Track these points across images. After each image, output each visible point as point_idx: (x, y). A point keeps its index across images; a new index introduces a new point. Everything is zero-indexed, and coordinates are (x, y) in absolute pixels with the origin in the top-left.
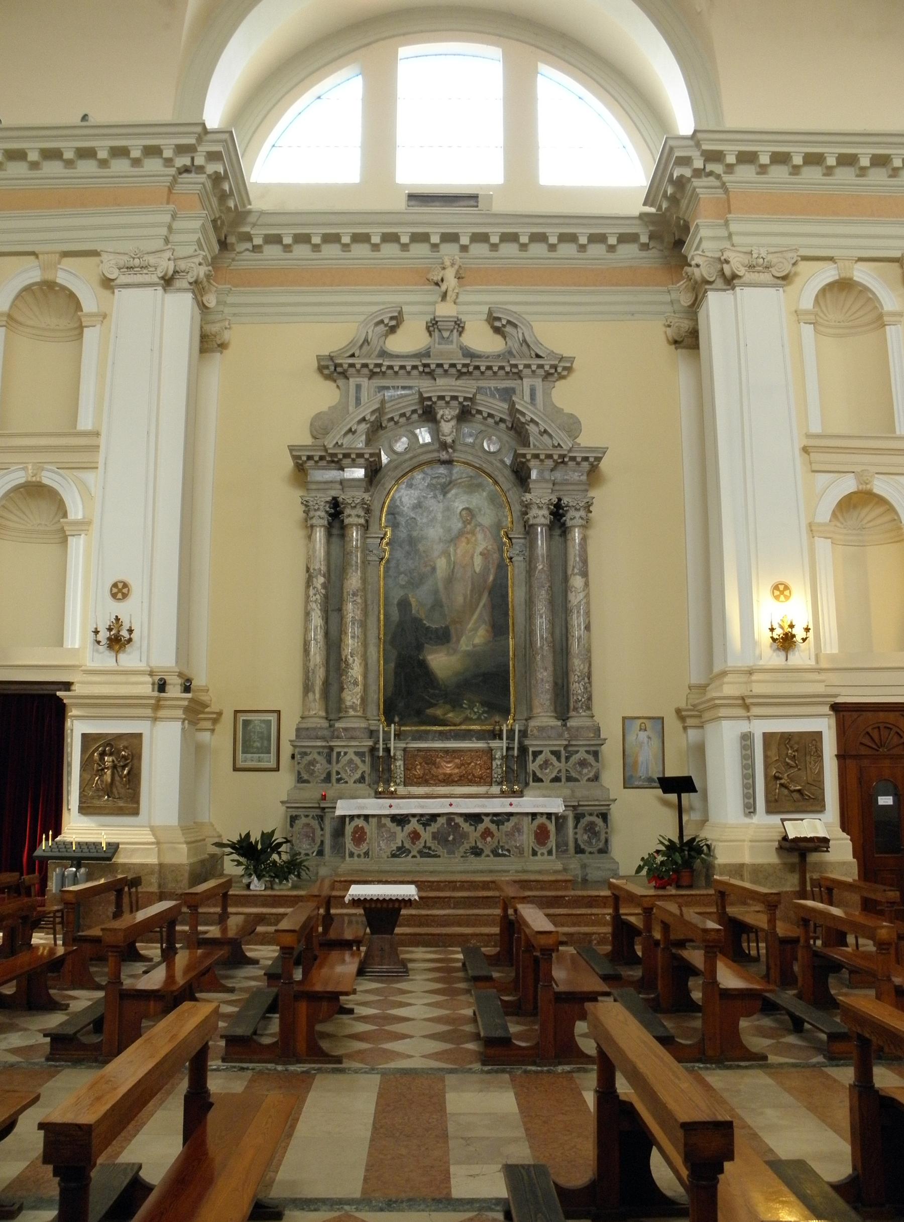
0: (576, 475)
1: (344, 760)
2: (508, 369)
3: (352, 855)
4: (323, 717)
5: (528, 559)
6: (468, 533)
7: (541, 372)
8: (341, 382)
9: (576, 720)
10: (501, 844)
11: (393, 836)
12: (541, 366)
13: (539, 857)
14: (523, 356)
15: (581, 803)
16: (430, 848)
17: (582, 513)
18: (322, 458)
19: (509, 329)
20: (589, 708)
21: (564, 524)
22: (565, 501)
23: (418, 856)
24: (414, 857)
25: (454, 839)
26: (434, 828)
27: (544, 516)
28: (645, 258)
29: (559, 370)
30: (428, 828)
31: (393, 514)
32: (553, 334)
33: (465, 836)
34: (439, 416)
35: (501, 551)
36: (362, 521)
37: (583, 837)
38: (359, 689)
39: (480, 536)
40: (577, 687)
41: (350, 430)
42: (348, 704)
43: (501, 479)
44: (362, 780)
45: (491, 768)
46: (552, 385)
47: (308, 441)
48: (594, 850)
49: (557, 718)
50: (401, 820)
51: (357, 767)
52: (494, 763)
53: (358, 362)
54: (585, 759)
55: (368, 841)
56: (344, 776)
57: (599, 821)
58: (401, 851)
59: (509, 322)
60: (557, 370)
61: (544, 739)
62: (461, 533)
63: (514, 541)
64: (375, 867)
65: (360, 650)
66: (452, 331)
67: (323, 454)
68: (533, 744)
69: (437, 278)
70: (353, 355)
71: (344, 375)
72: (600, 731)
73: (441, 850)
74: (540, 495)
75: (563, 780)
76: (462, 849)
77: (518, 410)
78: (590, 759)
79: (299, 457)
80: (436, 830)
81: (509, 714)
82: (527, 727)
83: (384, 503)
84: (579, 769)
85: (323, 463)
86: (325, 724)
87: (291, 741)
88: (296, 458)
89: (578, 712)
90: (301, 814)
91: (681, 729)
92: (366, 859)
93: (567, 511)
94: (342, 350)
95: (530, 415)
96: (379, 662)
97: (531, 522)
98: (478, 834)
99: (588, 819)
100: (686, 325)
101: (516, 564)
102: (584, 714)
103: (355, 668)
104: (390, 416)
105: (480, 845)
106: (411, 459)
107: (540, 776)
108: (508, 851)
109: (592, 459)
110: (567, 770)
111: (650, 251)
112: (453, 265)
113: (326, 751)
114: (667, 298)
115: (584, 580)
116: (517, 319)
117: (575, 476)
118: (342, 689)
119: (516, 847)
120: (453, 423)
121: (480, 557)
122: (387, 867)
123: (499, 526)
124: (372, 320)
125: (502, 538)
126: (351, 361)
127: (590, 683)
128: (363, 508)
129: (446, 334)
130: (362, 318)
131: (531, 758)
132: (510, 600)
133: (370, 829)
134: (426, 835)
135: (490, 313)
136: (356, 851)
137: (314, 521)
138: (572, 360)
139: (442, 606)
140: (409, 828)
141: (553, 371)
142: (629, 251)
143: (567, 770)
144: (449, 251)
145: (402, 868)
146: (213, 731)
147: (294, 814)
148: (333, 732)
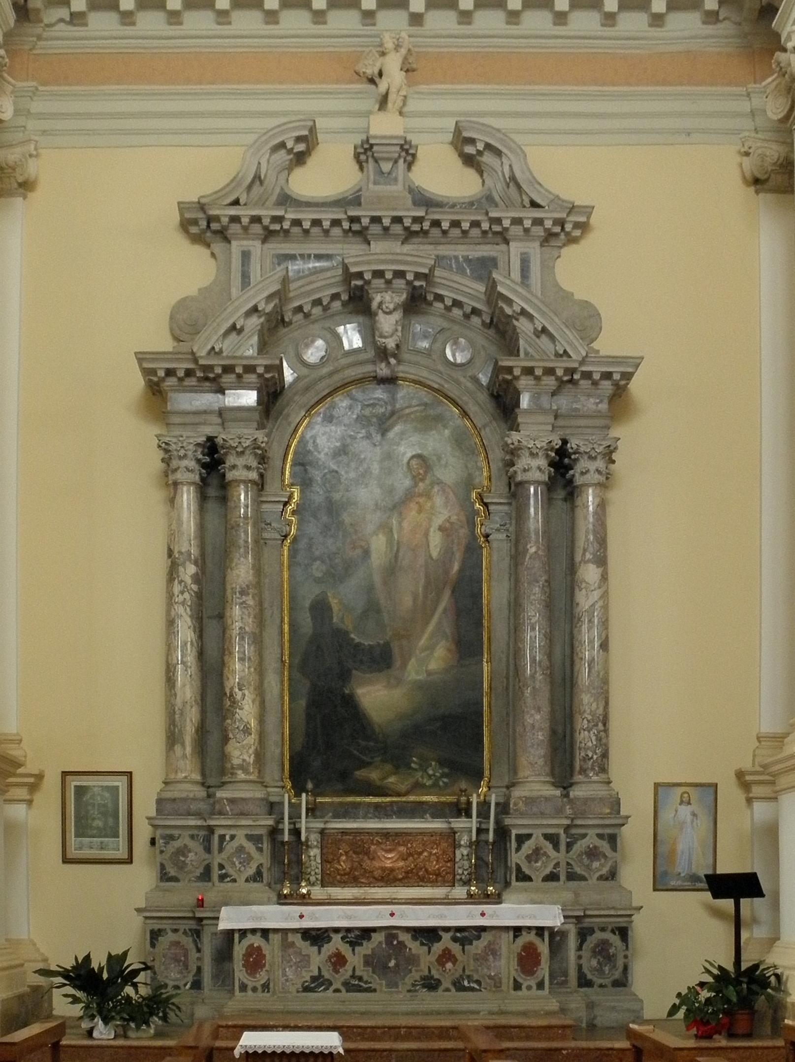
0: (591, 402)
1: (231, 847)
2: (485, 226)
3: (243, 988)
4: (197, 783)
5: (513, 537)
6: (420, 495)
7: (538, 231)
8: (218, 247)
9: (584, 787)
10: (467, 972)
11: (305, 960)
12: (538, 222)
13: (524, 992)
15: (588, 913)
16: (360, 979)
17: (600, 464)
18: (189, 373)
20: (603, 770)
21: (570, 482)
24: (337, 991)
25: (397, 965)
26: (366, 948)
28: (712, 37)
29: (568, 227)
30: (357, 949)
31: (302, 465)
32: (559, 169)
33: (413, 960)
35: (472, 524)
36: (254, 475)
37: (590, 963)
39: (439, 500)
40: (585, 739)
41: (233, 327)
42: (236, 762)
43: (472, 409)
44: (257, 877)
45: (453, 860)
46: (555, 253)
47: (167, 345)
49: (555, 785)
51: (250, 858)
52: (458, 852)
53: (245, 213)
54: (595, 847)
55: (267, 967)
56: (231, 871)
57: (615, 940)
58: (318, 983)
60: (565, 228)
61: (534, 816)
62: (410, 495)
63: (491, 508)
64: (279, 1006)
65: (254, 678)
66: (396, 162)
67: (191, 366)
68: (516, 824)
69: (372, 71)
70: (236, 202)
71: (223, 235)
73: (377, 982)
74: (535, 434)
75: (563, 877)
76: (409, 980)
77: (501, 295)
78: (604, 846)
79: (153, 372)
80: (369, 952)
83: (288, 446)
84: (586, 861)
86: (201, 793)
87: (149, 818)
88: (148, 373)
91: (744, 801)
92: (265, 994)
93: (576, 460)
95: (520, 303)
97: (519, 478)
98: (433, 958)
99: (599, 935)
101: (495, 545)
102: (595, 778)
103: (246, 707)
104: (296, 304)
105: (435, 974)
106: (331, 374)
108: (478, 982)
109: (616, 377)
110: (568, 864)
111: (720, 26)
112: (397, 47)
113: (202, 833)
115: (600, 570)
118: (226, 740)
119: (490, 977)
120: (397, 315)
123: (468, 484)
124: (266, 142)
125: (473, 504)
126: (233, 211)
127: (606, 731)
128: (256, 454)
129: (386, 167)
130: (250, 138)
131: (514, 845)
132: (485, 601)
133: (271, 950)
134: (355, 959)
135: (458, 131)
136: (250, 982)
137: (179, 476)
138: (588, 210)
139: (379, 611)
140: (329, 949)
141: (557, 229)
143: (568, 864)
145: (320, 1007)
146: (30, 802)
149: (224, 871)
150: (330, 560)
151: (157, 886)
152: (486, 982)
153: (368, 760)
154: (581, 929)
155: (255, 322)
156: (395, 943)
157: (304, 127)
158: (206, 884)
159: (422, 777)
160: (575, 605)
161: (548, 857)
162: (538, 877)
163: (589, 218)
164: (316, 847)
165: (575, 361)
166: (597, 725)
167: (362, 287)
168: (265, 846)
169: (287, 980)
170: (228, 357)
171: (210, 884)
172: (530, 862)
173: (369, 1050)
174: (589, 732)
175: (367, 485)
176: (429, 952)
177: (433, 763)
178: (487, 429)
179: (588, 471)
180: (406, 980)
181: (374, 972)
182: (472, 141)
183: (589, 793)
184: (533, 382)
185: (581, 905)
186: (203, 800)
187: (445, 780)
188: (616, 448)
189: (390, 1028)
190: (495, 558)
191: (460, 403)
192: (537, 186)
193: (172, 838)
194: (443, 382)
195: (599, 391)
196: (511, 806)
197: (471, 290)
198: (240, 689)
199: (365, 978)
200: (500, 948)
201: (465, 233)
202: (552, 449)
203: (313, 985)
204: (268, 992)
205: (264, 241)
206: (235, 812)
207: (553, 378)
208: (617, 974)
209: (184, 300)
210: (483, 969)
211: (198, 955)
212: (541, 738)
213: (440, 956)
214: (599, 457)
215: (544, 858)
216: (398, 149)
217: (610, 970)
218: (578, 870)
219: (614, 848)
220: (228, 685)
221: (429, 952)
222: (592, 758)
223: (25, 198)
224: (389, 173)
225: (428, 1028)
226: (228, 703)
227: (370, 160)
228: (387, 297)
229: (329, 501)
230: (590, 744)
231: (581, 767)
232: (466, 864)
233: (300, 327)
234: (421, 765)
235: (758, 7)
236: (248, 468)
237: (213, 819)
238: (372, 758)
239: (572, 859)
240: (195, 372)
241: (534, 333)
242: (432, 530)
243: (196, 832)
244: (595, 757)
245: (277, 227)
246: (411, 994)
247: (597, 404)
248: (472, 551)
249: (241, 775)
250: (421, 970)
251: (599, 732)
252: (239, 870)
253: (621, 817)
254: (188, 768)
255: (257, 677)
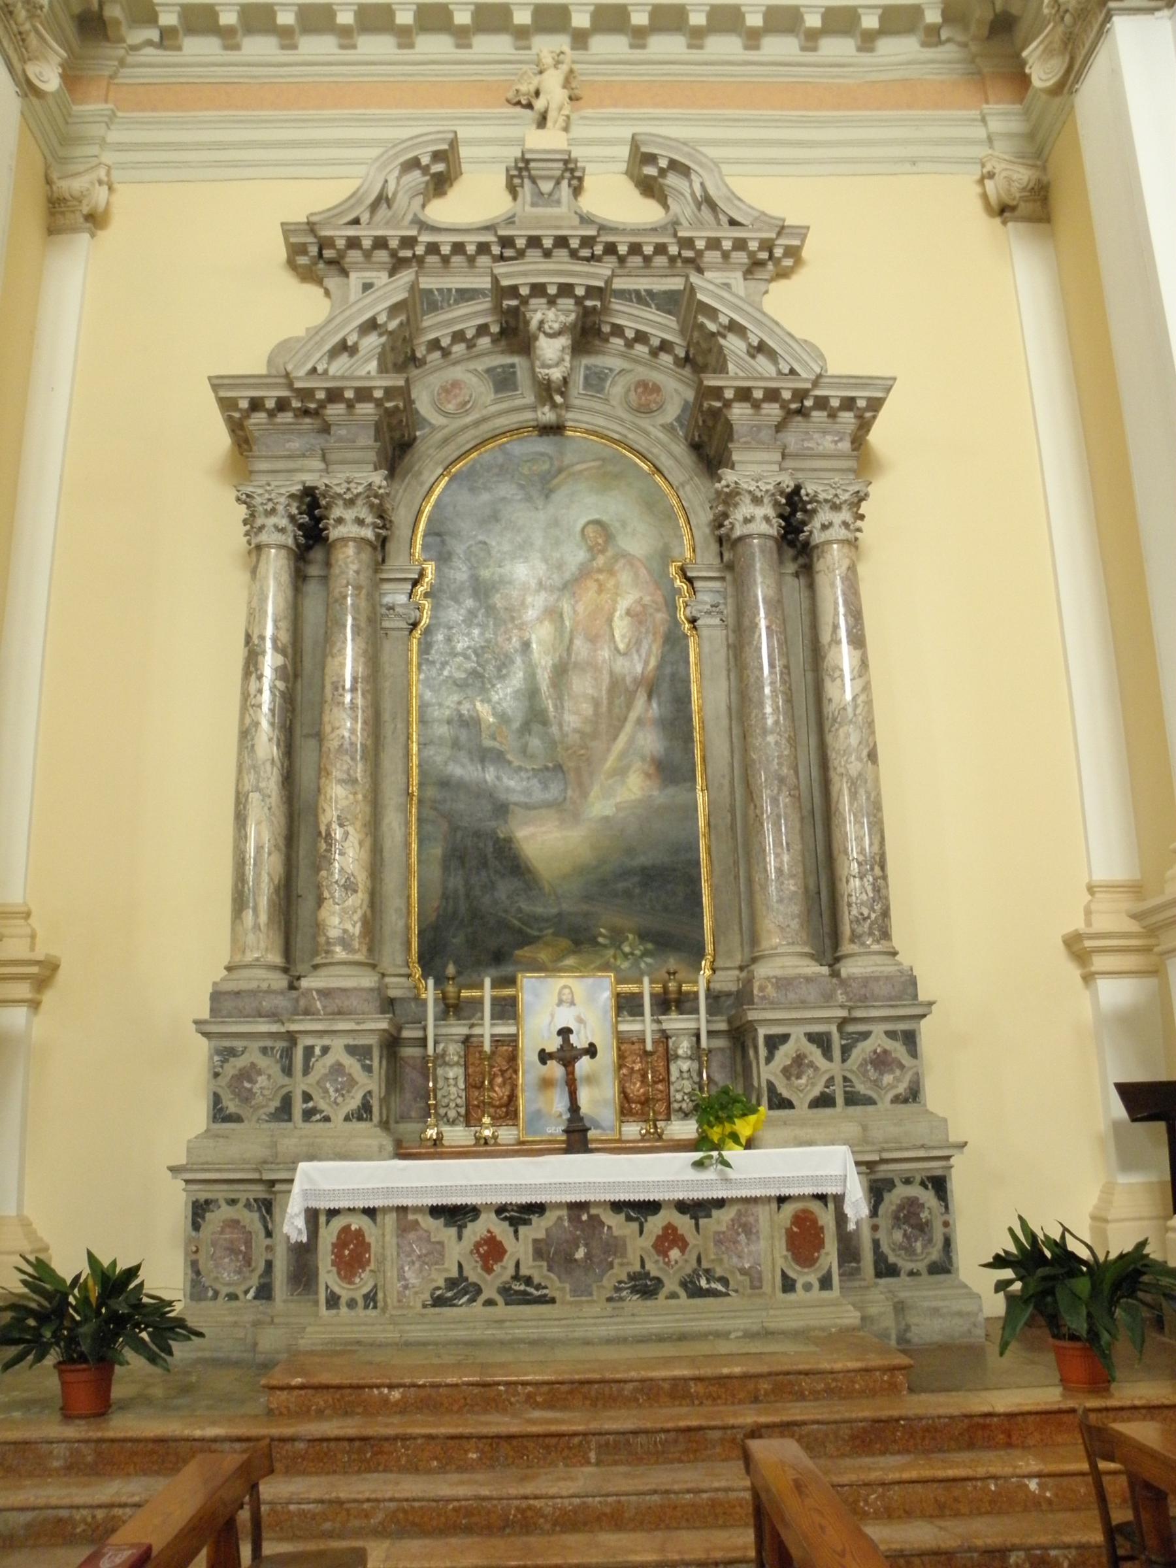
0: (825, 438)
1: (321, 1066)
2: (673, 250)
3: (333, 1301)
4: (273, 968)
5: (731, 621)
6: (600, 571)
7: (741, 257)
8: (333, 282)
9: (861, 961)
10: (705, 1265)
11: (437, 1251)
12: (740, 244)
13: (800, 1294)
14: (700, 224)
15: (886, 1155)
16: (528, 1281)
17: (845, 515)
18: (282, 405)
19: (672, 180)
20: (886, 935)
21: (806, 544)
22: (809, 489)
23: (499, 1299)
24: (490, 1303)
25: (588, 1256)
26: (538, 1228)
27: (767, 519)
28: (932, 61)
29: (778, 252)
30: (522, 1230)
31: (439, 534)
32: (762, 191)
33: (615, 1247)
34: (534, 324)
35: (672, 608)
36: (368, 533)
37: (892, 1238)
38: (358, 900)
39: (625, 577)
40: (855, 889)
42: (334, 933)
43: (665, 462)
44: (363, 1112)
45: (667, 1081)
46: (762, 286)
48: (921, 1266)
49: (817, 958)
50: (456, 1215)
51: (352, 1082)
52: (673, 1068)
53: (366, 234)
54: (885, 1052)
55: (372, 1266)
56: (322, 1105)
57: (928, 1197)
58: (459, 1288)
59: (674, 165)
60: (772, 255)
61: (791, 1007)
62: (584, 573)
63: (698, 584)
64: (390, 1334)
65: (362, 809)
66: (558, 183)
67: (285, 393)
68: (765, 1019)
69: (526, 87)
70: (356, 222)
71: (339, 266)
72: (915, 984)
73: (555, 1285)
74: (755, 471)
75: (840, 1100)
76: (609, 1282)
77: (701, 304)
78: (898, 1049)
80: (541, 1235)
81: (701, 954)
82: (749, 981)
83: (419, 512)
84: (872, 1073)
85: (287, 417)
86: (280, 981)
88: (227, 405)
89: (863, 944)
90: (221, 1196)
91: (1079, 980)
92: (371, 1313)
93: (814, 511)
94: (334, 213)
95: (727, 314)
96: (407, 845)
97: (738, 533)
98: (647, 1242)
99: (901, 1192)
100: (1023, 175)
101: (705, 632)
102: (875, 947)
103: (351, 853)
104: (432, 336)
105: (653, 1269)
106: (477, 423)
107: (786, 1094)
108: (724, 1281)
109: (861, 403)
110: (845, 1079)
111: (941, 49)
112: (557, 64)
113: (280, 1044)
114: (980, 132)
115: (858, 653)
116: (689, 155)
117: (827, 443)
118: (320, 901)
119: (743, 1272)
120: (564, 341)
121: (627, 620)
122: (416, 1332)
123: (665, 557)
124: (396, 155)
125: (672, 581)
126: (352, 232)
127: (885, 878)
128: (372, 506)
129: (546, 187)
130: (375, 152)
131: (763, 1052)
132: (695, 707)
133: (381, 1237)
134: (519, 1247)
135: (635, 144)
136: (344, 1291)
137: (264, 538)
138: (802, 232)
139: (545, 723)
140: (476, 1230)
141: (764, 255)
142: (900, 49)
143: (845, 1079)
144: (547, 46)
145: (461, 1334)
146: (34, 1005)
147: (203, 1197)
148: (297, 1000)
149: (311, 1104)
150: (477, 655)
151: (207, 1131)
152: (736, 1280)
153: (536, 933)
154: (876, 1181)
155: (373, 341)
156: (585, 1217)
157: (443, 140)
158: (283, 1125)
159: (615, 957)
160: (825, 702)
161: (816, 1069)
162: (801, 1102)
163: (803, 240)
164: (457, 1063)
165: (806, 380)
166: (872, 869)
167: (517, 308)
168: (376, 1064)
169: (406, 1287)
170: (334, 378)
171: (290, 1125)
172: (788, 1078)
173: (546, 1436)
174: (861, 878)
175: (526, 560)
176: (641, 1232)
177: (631, 936)
178: (688, 488)
179: (831, 524)
180: (605, 1282)
181: (550, 1269)
182: (651, 159)
183: (869, 970)
184: (750, 411)
185: (873, 1144)
186: (282, 993)
187: (649, 960)
188: (867, 495)
189: (582, 1383)
190: (706, 649)
191: (650, 456)
192: (737, 202)
193: (231, 1052)
194: (625, 432)
195: (837, 426)
196: (756, 992)
197: (661, 325)
198: (341, 825)
199: (536, 1281)
200: (757, 1221)
201: (647, 259)
202: (782, 493)
203: (449, 1294)
204: (375, 1307)
205: (392, 272)
206: (329, 1010)
207: (777, 405)
208: (935, 1254)
209: (286, 341)
210: (730, 1257)
211: (268, 1241)
212: (793, 888)
213: (658, 1237)
214: (845, 507)
215: (810, 1071)
216: (561, 165)
217: (924, 1247)
218: (861, 1088)
219: (913, 1052)
220: (324, 820)
221: (641, 1232)
222: (869, 917)
223: (93, 236)
224: (550, 194)
225: (651, 1380)
226: (324, 846)
227: (526, 181)
228: (551, 314)
229: (475, 579)
230: (864, 897)
231: (853, 931)
232: (687, 1086)
233: (438, 369)
234: (612, 939)
235: (991, 16)
236: (360, 522)
237: (294, 1021)
238: (540, 930)
239: (851, 1071)
240: (290, 404)
241: (748, 353)
242: (617, 614)
243: (269, 1043)
244: (873, 916)
245: (408, 253)
246: (612, 1304)
247: (836, 442)
248: (674, 641)
249: (340, 953)
250: (628, 1264)
251: (875, 879)
252: (335, 1103)
253: (921, 1004)
254: (262, 945)
255: (368, 809)
